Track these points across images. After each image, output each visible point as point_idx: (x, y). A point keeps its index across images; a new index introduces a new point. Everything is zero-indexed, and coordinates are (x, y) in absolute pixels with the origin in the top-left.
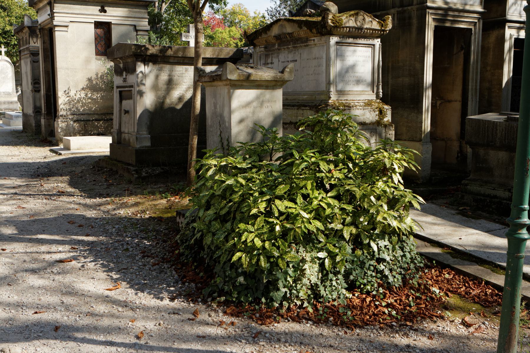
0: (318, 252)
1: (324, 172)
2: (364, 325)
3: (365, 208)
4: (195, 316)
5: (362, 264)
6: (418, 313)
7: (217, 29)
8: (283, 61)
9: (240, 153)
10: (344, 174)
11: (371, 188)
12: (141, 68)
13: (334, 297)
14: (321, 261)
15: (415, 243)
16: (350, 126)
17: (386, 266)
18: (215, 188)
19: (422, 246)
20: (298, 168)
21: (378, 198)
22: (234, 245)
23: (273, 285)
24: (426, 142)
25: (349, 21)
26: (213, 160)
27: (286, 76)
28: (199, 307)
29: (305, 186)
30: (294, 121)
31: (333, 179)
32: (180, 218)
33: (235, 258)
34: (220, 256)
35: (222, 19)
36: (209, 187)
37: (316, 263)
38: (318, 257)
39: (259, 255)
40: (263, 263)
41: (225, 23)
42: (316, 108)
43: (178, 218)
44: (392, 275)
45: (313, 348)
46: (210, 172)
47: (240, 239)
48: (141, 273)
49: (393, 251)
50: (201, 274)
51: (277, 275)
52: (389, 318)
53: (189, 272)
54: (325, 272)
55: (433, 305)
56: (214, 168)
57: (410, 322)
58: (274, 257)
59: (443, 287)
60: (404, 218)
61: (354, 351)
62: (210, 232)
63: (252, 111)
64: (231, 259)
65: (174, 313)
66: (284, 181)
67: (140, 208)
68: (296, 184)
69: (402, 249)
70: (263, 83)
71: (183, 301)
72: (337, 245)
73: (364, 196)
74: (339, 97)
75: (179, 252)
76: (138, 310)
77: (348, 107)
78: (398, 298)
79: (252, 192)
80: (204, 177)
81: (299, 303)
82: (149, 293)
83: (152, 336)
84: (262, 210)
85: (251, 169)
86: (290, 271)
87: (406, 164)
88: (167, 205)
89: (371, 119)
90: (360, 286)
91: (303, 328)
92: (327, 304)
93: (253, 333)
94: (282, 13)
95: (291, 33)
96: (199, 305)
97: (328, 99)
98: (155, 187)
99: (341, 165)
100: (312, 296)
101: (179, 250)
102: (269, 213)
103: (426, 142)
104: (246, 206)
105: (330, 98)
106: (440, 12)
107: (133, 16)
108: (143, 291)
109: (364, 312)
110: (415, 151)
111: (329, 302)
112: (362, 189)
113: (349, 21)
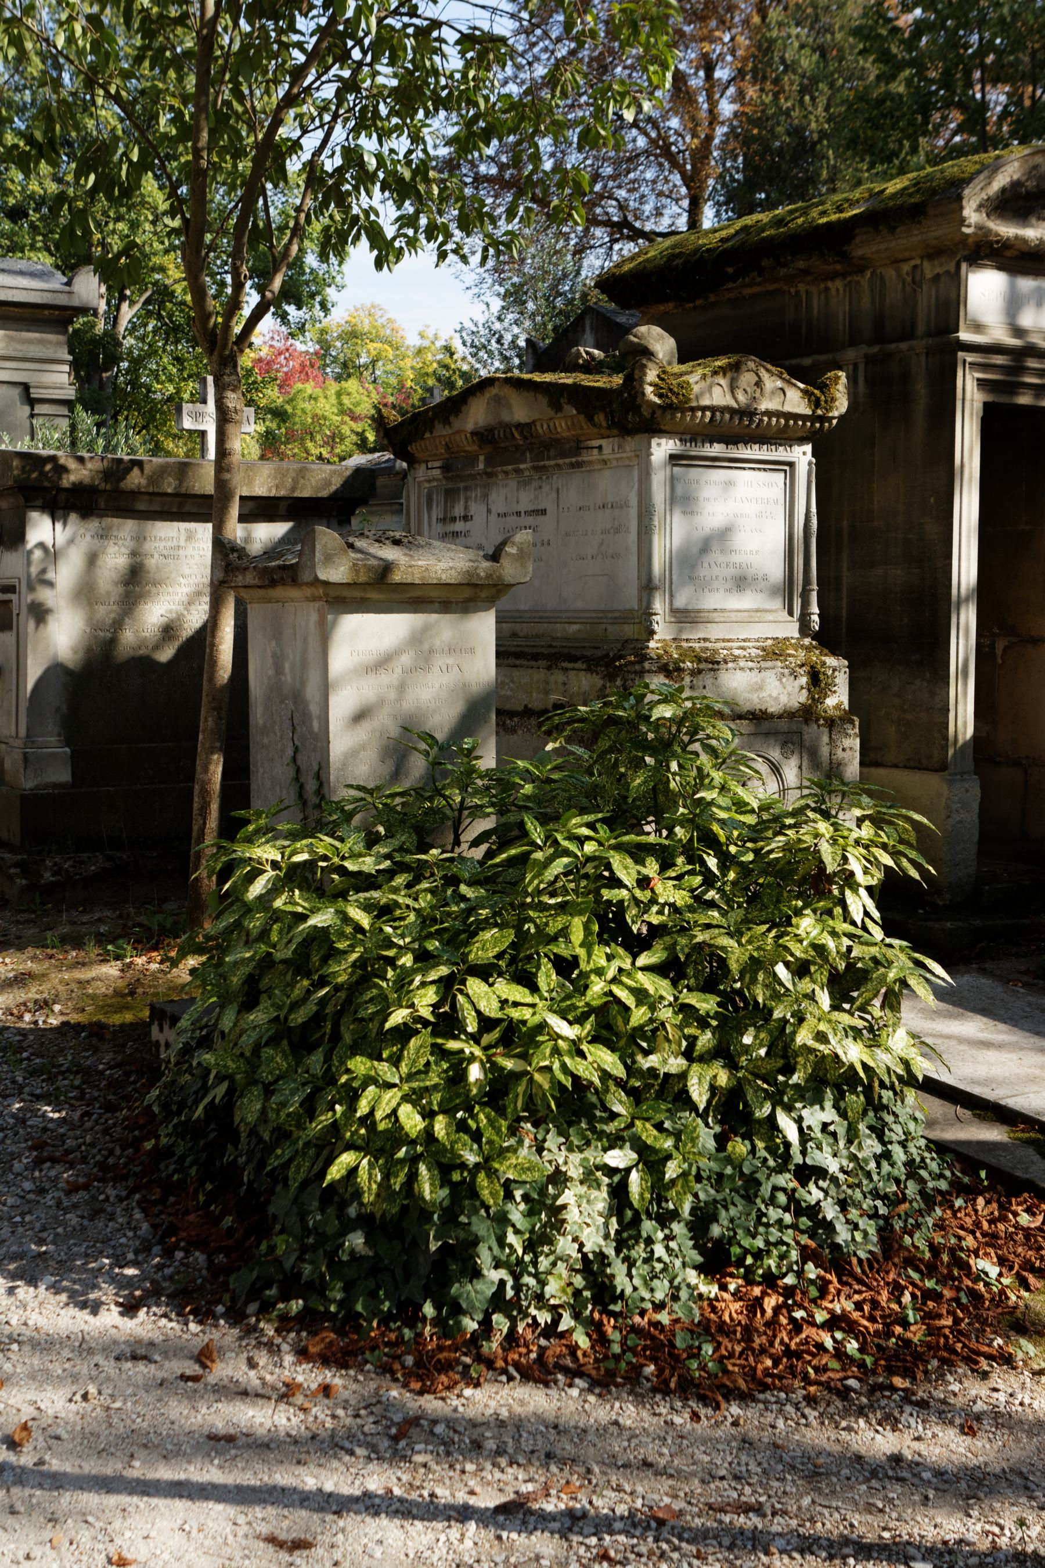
0: (605, 1150)
1: (625, 887)
2: (753, 1389)
3: (757, 1003)
4: (204, 1366)
5: (750, 1187)
6: (929, 1346)
7: (299, 386)
8: (502, 511)
9: (357, 820)
10: (692, 891)
11: (778, 937)
12: (42, 530)
13: (659, 1296)
14: (616, 1179)
15: (922, 1110)
16: (709, 737)
17: (826, 1192)
18: (274, 937)
19: (948, 1123)
20: (540, 874)
21: (801, 970)
22: (335, 1127)
23: (461, 1260)
24: (962, 773)
25: (711, 390)
26: (267, 848)
27: (509, 570)
28: (216, 1335)
29: (564, 933)
30: (536, 704)
31: (655, 909)
32: (161, 1030)
33: (335, 1172)
34: (290, 1160)
35: (316, 353)
36: (255, 933)
37: (599, 1187)
38: (606, 1165)
39: (413, 1160)
40: (428, 1188)
41: (326, 365)
42: (607, 666)
43: (155, 1029)
44: (848, 1222)
45: (589, 1471)
46: (257, 888)
47: (352, 1108)
48: (28, 1218)
49: (850, 1142)
50: (228, 1221)
51: (474, 1228)
52: (834, 1364)
53: (187, 1213)
54: (629, 1213)
55: (978, 1318)
56: (270, 873)
57: (904, 1377)
58: (463, 1166)
59: (1011, 1257)
60: (884, 1034)
61: (722, 1478)
62: (256, 1082)
63: (395, 683)
64: (323, 1173)
65: (135, 1358)
66: (495, 914)
67: (32, 993)
68: (537, 926)
69: (879, 1132)
70: (434, 594)
71: (165, 1315)
72: (667, 1125)
73: (754, 965)
74: (680, 631)
75: (156, 1145)
76: (15, 1347)
77: (710, 663)
78: (867, 1295)
79: (391, 953)
80: (238, 899)
81: (544, 1317)
82: (56, 1289)
83: (58, 1438)
84: (426, 1013)
85: (390, 874)
86: (517, 1213)
87: (887, 860)
88: (120, 983)
89: (784, 699)
90: (740, 1262)
91: (556, 1404)
92: (637, 1319)
93: (393, 1424)
94: (508, 338)
95: (528, 425)
96: (216, 1326)
97: (644, 636)
98: (85, 918)
99: (680, 860)
100: (587, 1294)
101: (158, 1137)
102: (447, 1022)
103: (962, 773)
104: (371, 1000)
105: (652, 633)
106: (999, 360)
107: (20, 355)
108: (33, 1282)
109: (756, 1345)
110: (917, 817)
111: (642, 1313)
112: (749, 942)
113: (711, 387)
